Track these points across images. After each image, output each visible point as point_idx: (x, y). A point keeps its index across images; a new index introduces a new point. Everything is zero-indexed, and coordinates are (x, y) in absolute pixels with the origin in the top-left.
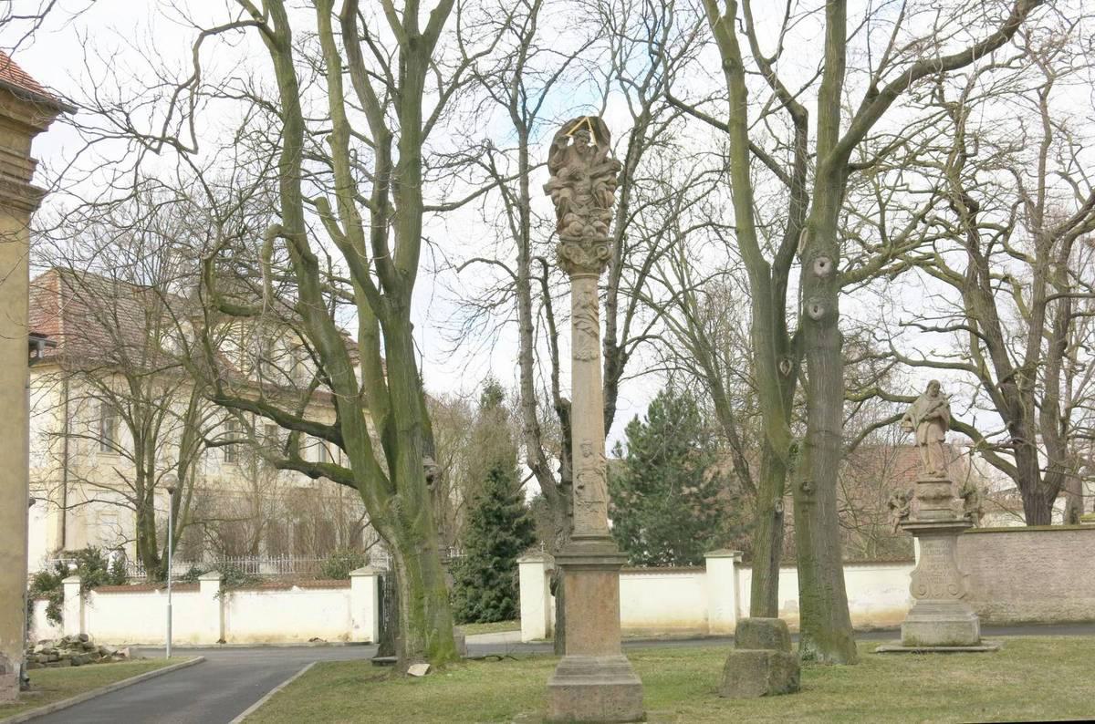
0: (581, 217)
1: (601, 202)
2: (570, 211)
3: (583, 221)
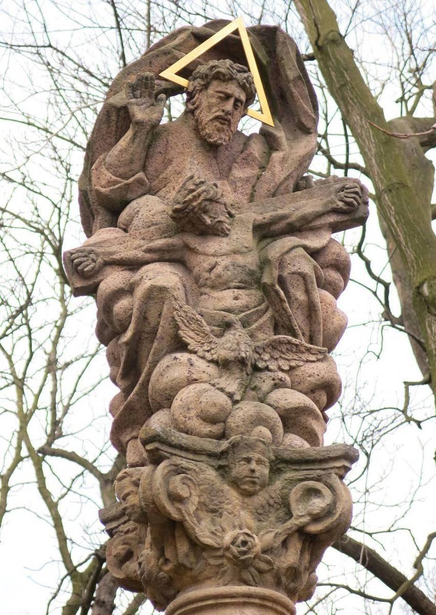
0: (223, 365)
1: (299, 320)
2: (182, 346)
3: (232, 384)
